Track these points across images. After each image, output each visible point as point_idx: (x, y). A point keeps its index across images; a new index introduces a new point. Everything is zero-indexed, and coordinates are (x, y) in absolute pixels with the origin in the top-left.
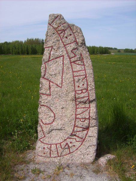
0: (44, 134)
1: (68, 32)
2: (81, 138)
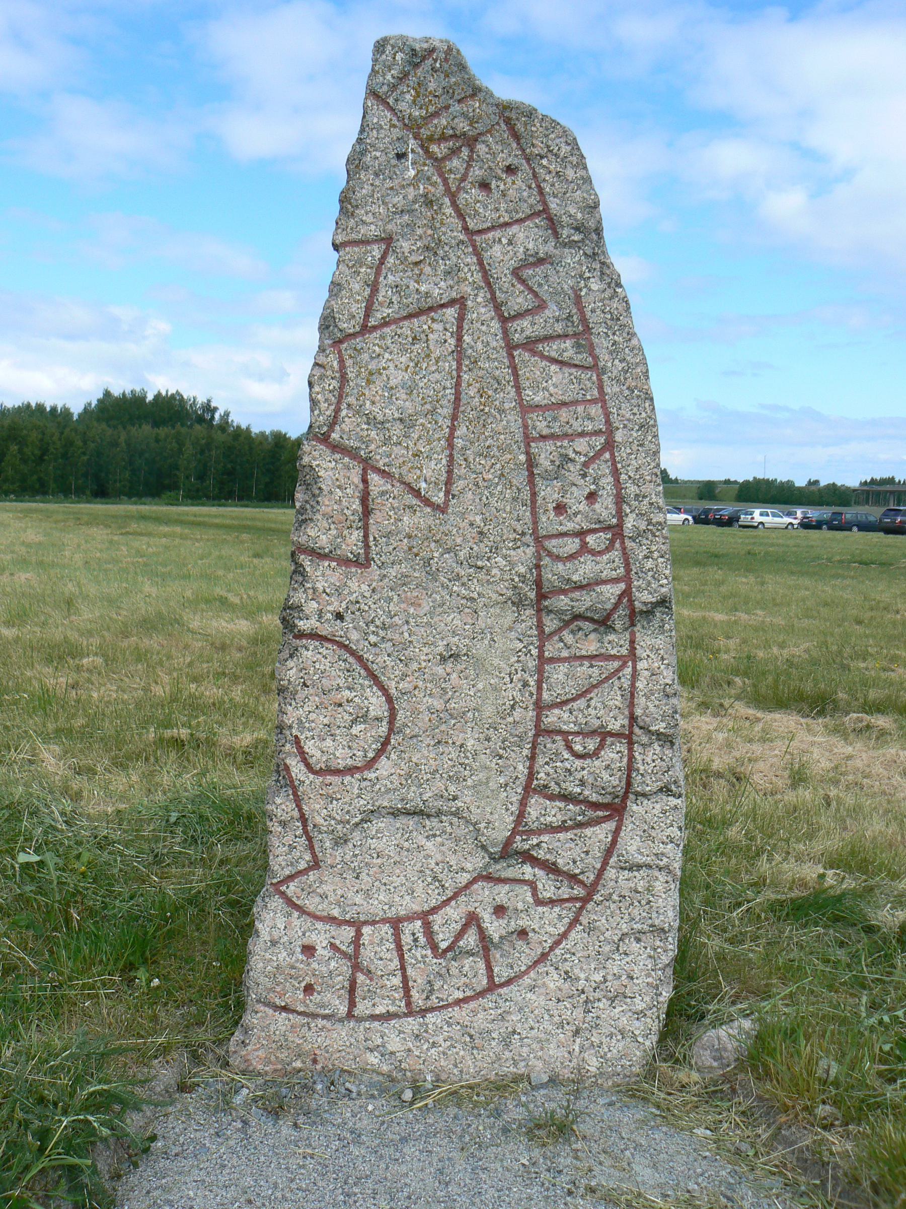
0: (311, 847)
1: (496, 151)
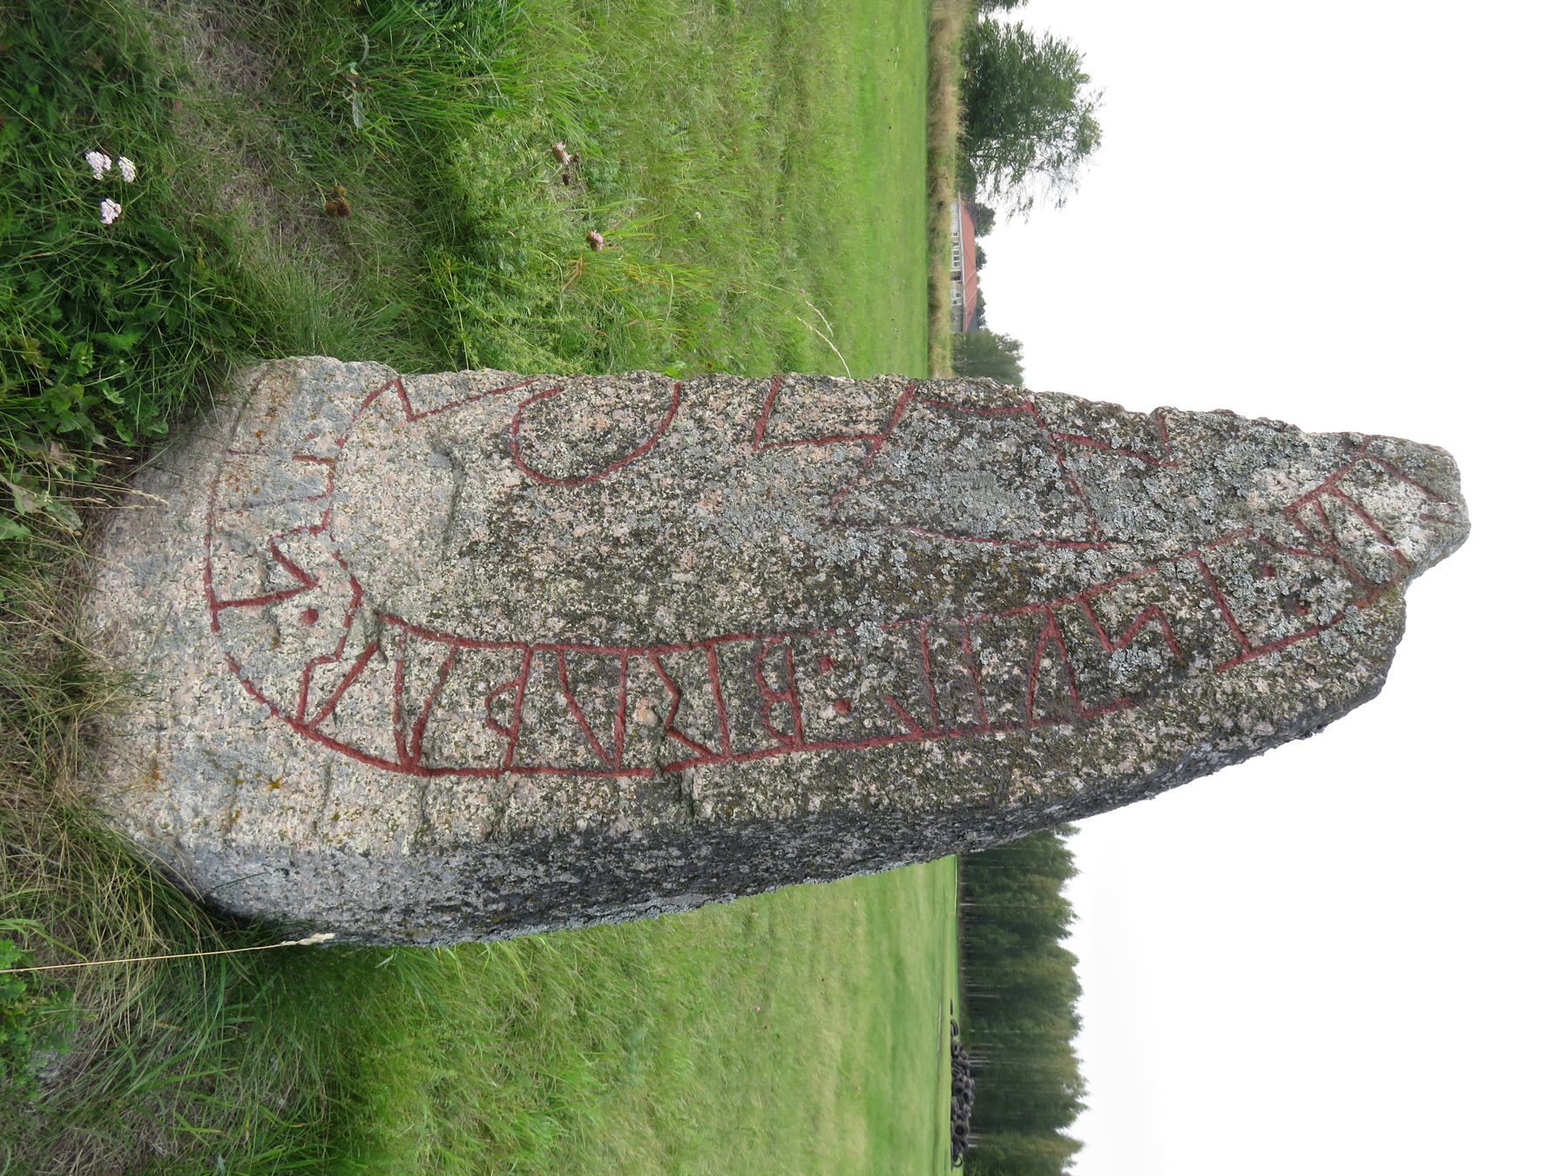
2: (329, 707)
